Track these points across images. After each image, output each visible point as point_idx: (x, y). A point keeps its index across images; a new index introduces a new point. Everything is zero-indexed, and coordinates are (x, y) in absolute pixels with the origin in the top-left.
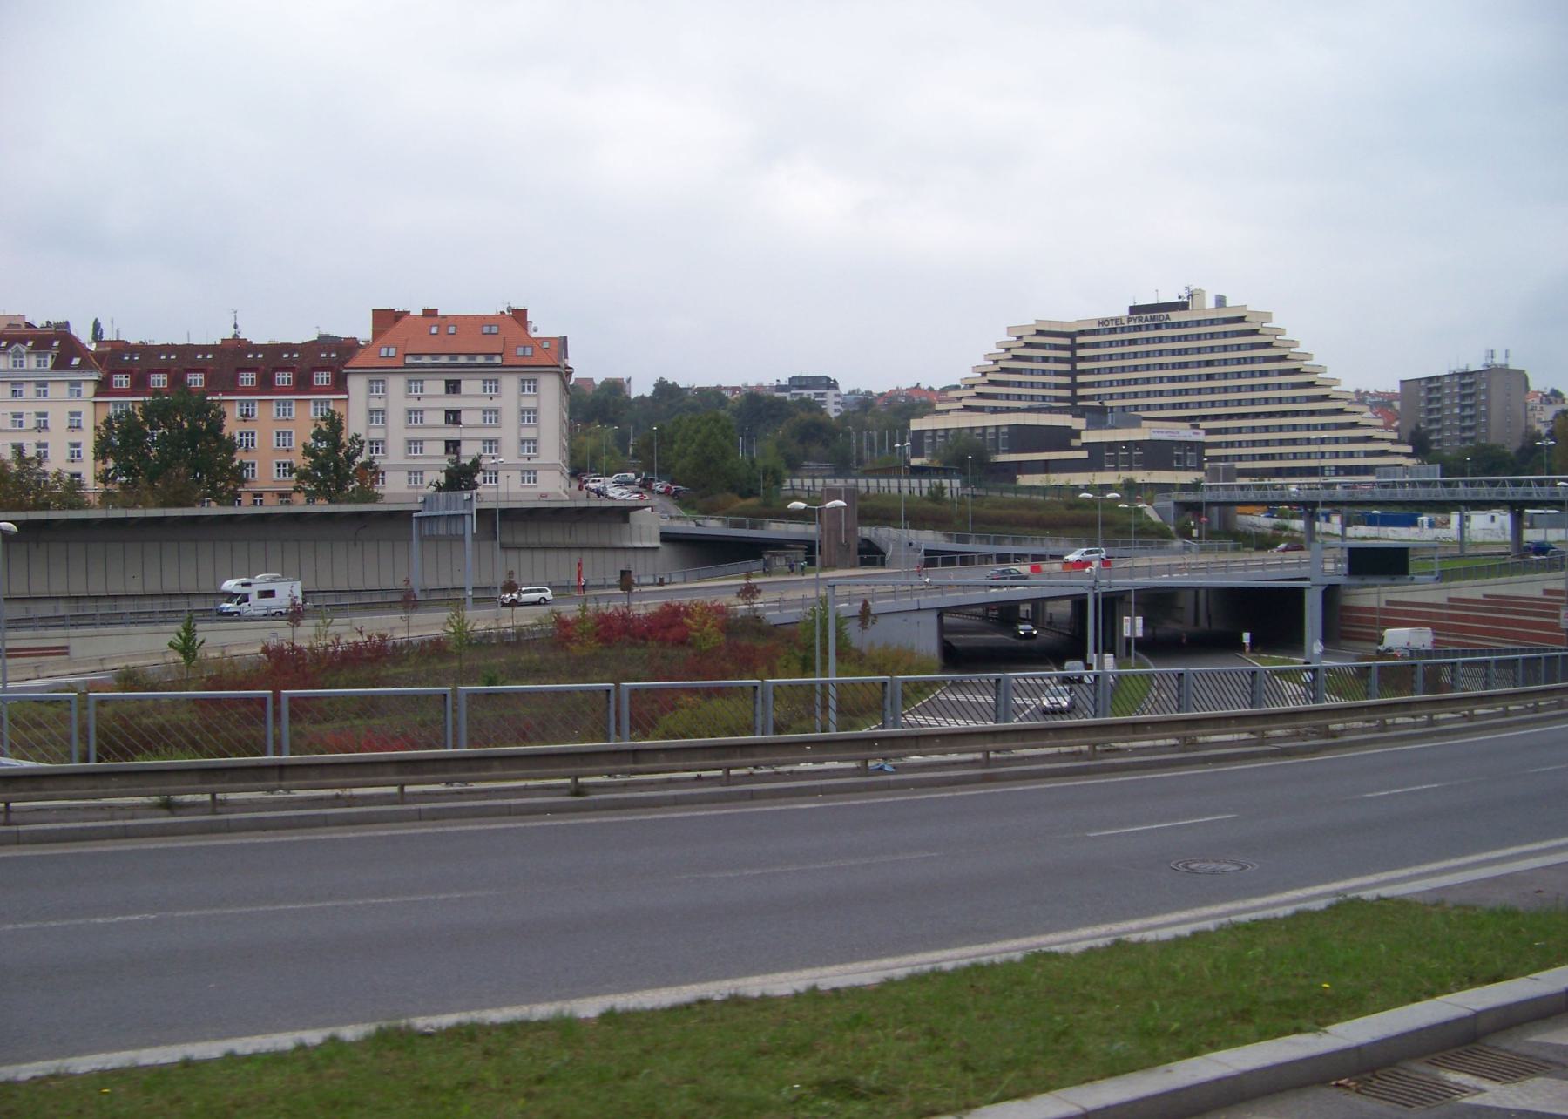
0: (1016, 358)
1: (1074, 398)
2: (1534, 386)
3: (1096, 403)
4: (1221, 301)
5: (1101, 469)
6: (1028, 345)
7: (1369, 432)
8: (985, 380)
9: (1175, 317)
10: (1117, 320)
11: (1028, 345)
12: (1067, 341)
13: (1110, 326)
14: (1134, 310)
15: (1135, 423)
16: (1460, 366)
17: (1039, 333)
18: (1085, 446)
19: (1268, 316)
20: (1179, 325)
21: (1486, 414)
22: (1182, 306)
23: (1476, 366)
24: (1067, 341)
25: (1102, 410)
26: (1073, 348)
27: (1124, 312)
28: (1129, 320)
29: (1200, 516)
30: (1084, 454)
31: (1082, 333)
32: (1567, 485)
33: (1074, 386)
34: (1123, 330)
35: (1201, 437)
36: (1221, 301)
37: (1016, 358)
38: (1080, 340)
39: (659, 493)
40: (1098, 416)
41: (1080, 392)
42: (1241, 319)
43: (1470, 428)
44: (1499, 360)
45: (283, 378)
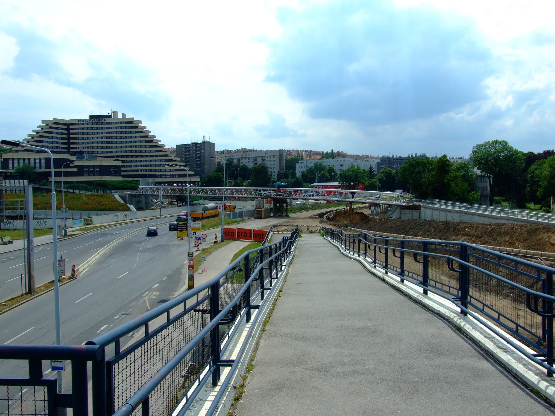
0: (46, 132)
1: (69, 148)
2: (217, 149)
3: (79, 150)
4: (124, 115)
5: (83, 175)
6: (50, 128)
7: (176, 163)
8: (33, 140)
9: (108, 120)
10: (85, 120)
11: (50, 128)
12: (66, 127)
13: (82, 122)
14: (91, 117)
15: (95, 158)
16: (195, 141)
17: (55, 123)
18: (75, 167)
19: (140, 122)
20: (109, 123)
21: (204, 156)
22: (109, 116)
23: (200, 141)
24: (66, 127)
25: (82, 153)
26: (68, 129)
27: (88, 118)
28: (90, 120)
29: (183, 203)
30: (76, 170)
31: (72, 124)
32: (554, 238)
33: (69, 144)
34: (88, 124)
35: (119, 164)
36: (124, 115)
37: (46, 132)
38: (71, 127)
39: (225, 282)
40: (80, 155)
41: (71, 146)
42: (131, 122)
43: (199, 161)
44: (207, 139)
45: (361, 372)
